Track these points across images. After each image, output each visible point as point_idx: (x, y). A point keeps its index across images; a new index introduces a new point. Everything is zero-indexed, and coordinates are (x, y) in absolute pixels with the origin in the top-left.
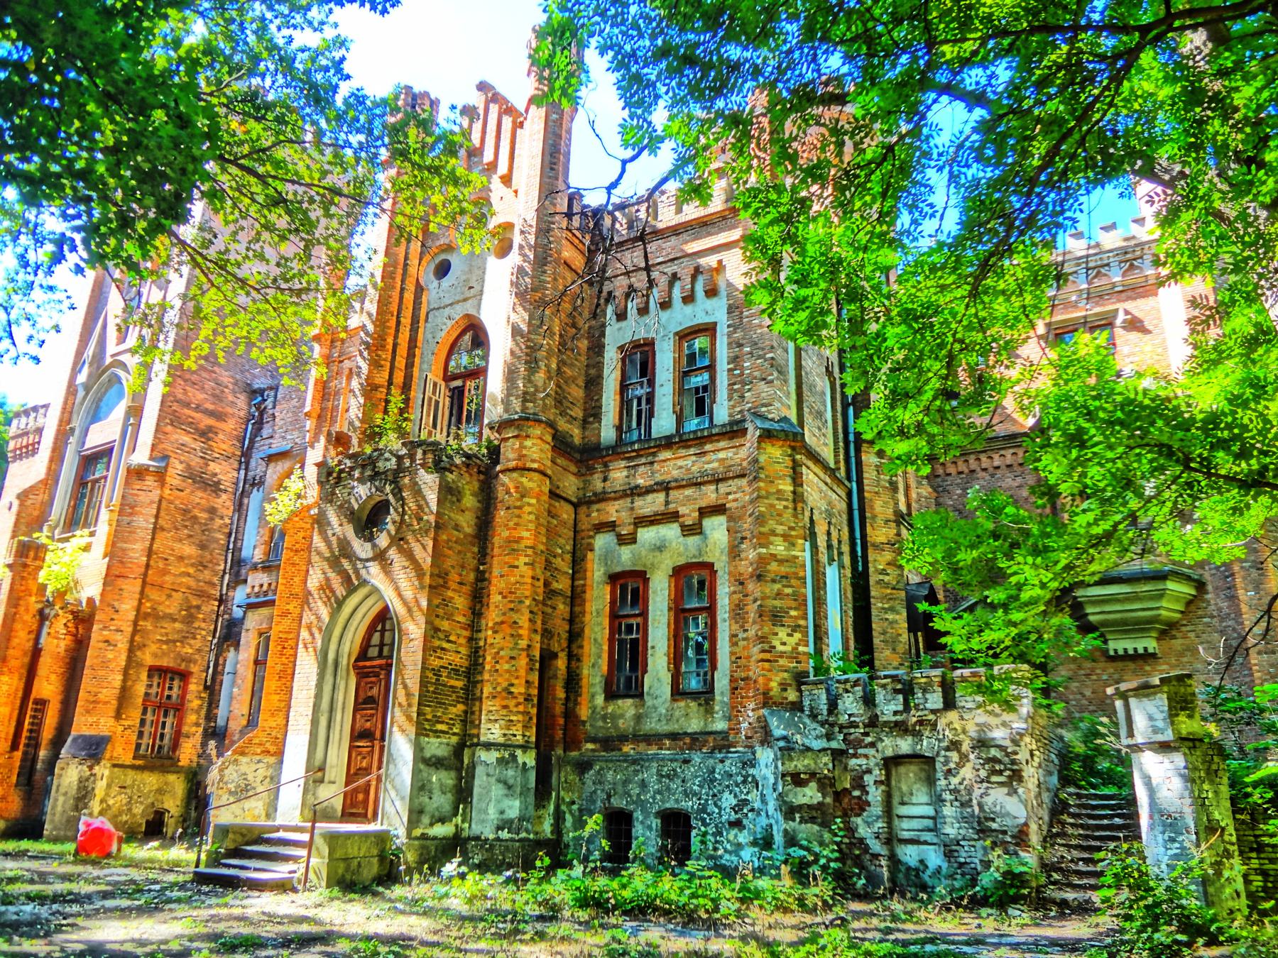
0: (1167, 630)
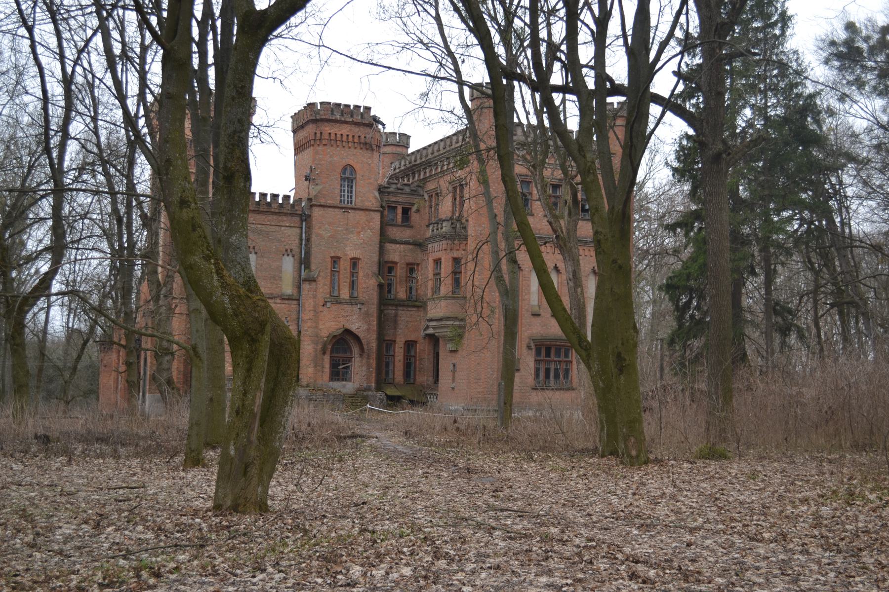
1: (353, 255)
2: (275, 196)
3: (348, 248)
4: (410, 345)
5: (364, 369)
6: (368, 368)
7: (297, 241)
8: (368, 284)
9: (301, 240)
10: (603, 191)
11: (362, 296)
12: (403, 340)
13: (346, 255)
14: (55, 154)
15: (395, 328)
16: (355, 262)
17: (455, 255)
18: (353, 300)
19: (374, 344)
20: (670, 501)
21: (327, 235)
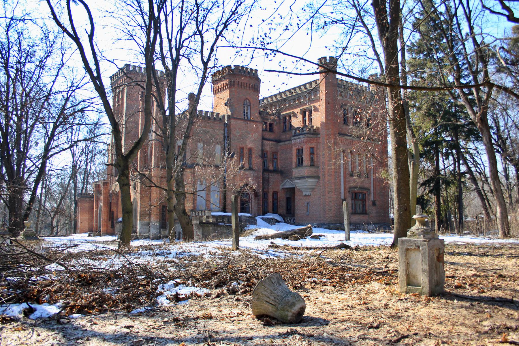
0: (313, 189)
1: (249, 146)
2: (207, 112)
3: (248, 142)
4: (275, 193)
5: (256, 206)
6: (258, 205)
7: (222, 137)
8: (257, 161)
9: (225, 137)
10: (140, 131)
11: (255, 168)
12: (272, 191)
13: (247, 146)
14: (153, 81)
15: (268, 185)
16: (250, 150)
17: (311, 146)
18: (250, 169)
19: (261, 193)
20: (193, 345)
21: (238, 135)
